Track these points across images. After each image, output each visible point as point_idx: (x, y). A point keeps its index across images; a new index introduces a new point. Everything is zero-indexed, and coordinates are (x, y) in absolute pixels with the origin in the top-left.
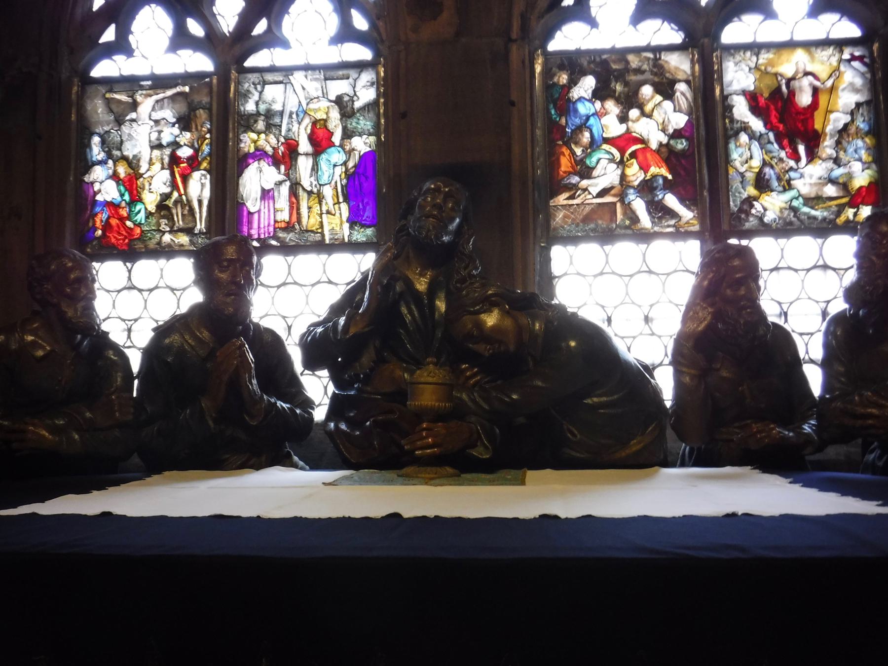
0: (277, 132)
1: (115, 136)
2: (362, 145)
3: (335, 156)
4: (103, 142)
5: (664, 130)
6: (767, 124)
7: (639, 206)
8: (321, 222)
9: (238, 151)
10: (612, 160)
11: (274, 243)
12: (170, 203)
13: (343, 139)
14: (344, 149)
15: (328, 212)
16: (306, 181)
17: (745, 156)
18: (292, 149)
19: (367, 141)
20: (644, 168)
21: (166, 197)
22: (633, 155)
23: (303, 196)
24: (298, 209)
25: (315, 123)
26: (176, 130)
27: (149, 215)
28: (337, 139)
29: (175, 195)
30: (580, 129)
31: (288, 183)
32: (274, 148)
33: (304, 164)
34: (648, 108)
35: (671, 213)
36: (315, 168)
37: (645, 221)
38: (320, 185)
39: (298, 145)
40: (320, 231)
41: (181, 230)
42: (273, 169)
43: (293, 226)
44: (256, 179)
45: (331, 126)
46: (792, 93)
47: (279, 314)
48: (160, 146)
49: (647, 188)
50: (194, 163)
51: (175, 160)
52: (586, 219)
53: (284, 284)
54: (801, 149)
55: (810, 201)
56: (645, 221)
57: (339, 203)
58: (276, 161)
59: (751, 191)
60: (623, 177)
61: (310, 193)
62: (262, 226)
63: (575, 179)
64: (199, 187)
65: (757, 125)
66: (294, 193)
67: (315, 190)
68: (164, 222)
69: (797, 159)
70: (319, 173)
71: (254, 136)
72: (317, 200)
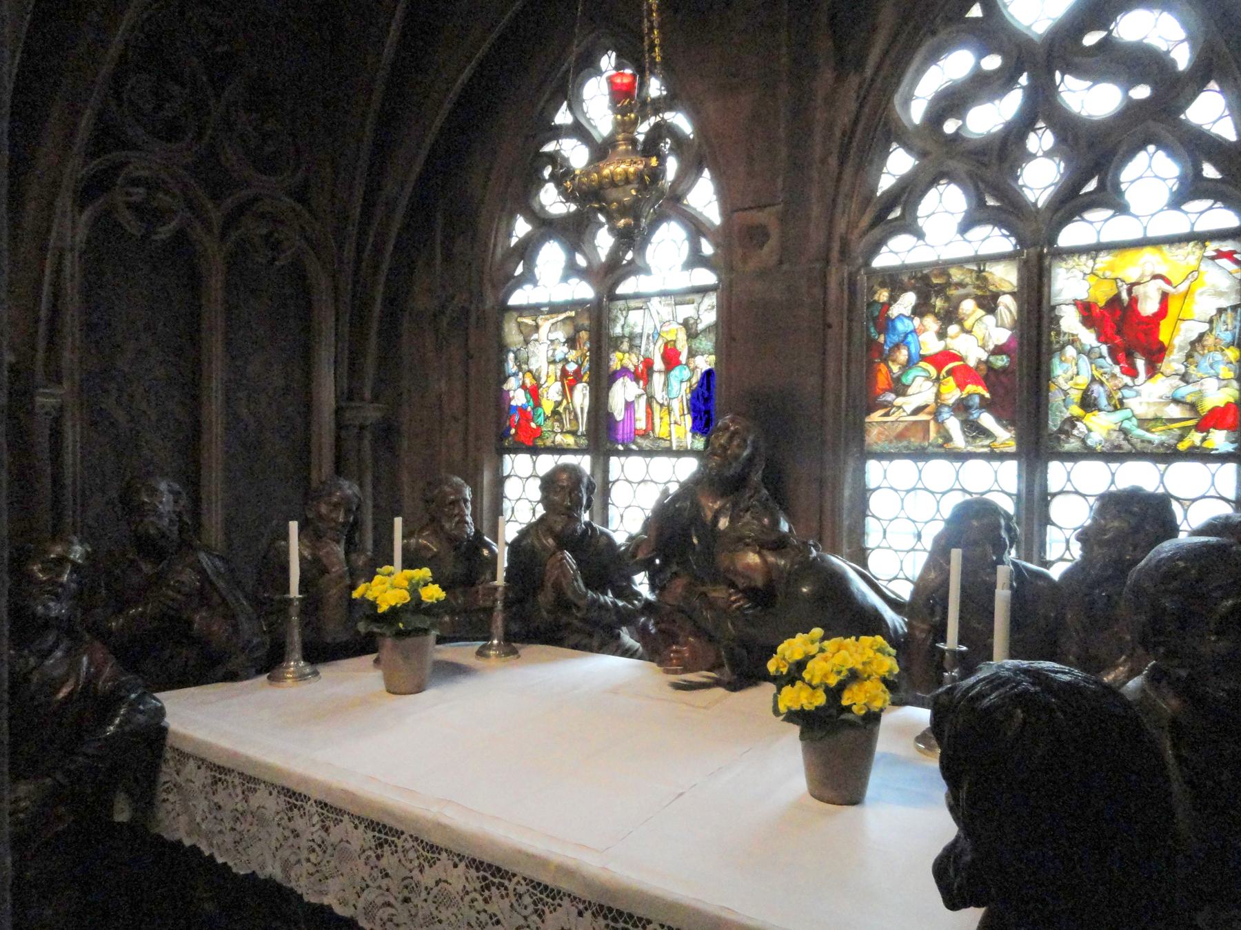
1: (523, 354)
2: (705, 363)
3: (678, 373)
4: (516, 358)
5: (983, 347)
6: (1101, 338)
7: (953, 425)
10: (928, 378)
11: (634, 447)
12: (561, 409)
16: (659, 394)
17: (1070, 373)
18: (648, 363)
20: (961, 386)
21: (558, 404)
22: (949, 373)
23: (656, 407)
25: (666, 345)
26: (565, 349)
27: (547, 418)
28: (683, 358)
29: (565, 402)
30: (897, 346)
33: (658, 379)
34: (967, 324)
35: (986, 433)
36: (666, 384)
37: (959, 441)
41: (568, 432)
44: (622, 393)
45: (679, 347)
46: (1134, 301)
48: (554, 362)
49: (962, 407)
50: (577, 377)
51: (564, 373)
52: (901, 436)
54: (1140, 363)
55: (1143, 422)
56: (959, 441)
58: (636, 377)
59: (1076, 410)
60: (938, 395)
61: (662, 405)
63: (890, 397)
64: (581, 397)
65: (1088, 337)
68: (557, 424)
69: (1133, 373)
71: (619, 355)
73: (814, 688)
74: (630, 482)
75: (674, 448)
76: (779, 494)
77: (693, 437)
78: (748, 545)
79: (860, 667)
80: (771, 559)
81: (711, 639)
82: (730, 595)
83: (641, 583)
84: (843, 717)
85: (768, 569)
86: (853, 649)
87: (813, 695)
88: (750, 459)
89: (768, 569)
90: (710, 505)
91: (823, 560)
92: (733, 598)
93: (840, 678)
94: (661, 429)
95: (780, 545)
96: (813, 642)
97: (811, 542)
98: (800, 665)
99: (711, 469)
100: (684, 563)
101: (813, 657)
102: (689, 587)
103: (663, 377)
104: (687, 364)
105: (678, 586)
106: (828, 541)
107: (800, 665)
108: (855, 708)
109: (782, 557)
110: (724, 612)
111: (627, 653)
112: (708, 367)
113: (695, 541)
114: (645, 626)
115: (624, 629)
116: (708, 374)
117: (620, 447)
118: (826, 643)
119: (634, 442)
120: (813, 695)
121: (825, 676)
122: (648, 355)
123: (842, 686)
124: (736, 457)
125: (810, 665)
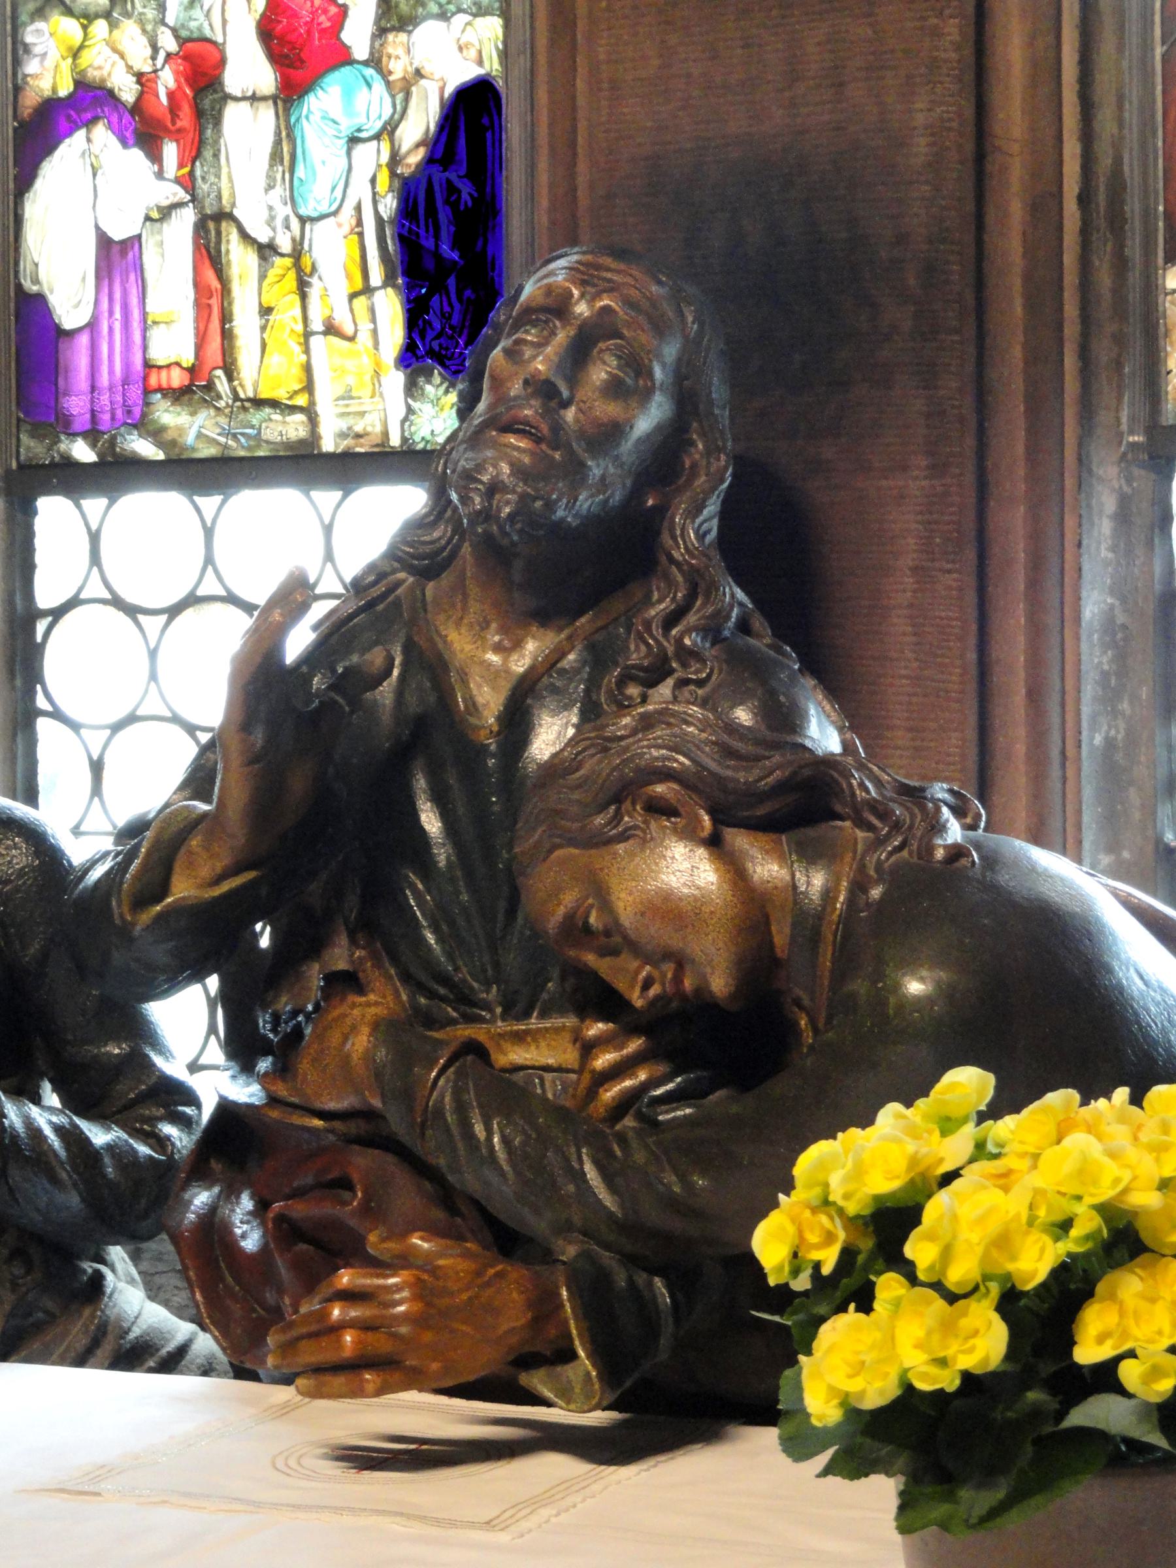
0: (151, 13)
3: (339, 103)
8: (308, 369)
9: (17, 90)
11: (145, 448)
13: (381, 32)
14: (384, 74)
15: (331, 329)
18: (202, 70)
19: (469, 36)
23: (241, 260)
24: (226, 317)
28: (357, 34)
31: (187, 218)
32: (140, 77)
33: (245, 131)
36: (285, 153)
38: (303, 220)
39: (222, 62)
40: (302, 400)
42: (136, 155)
43: (210, 387)
47: (176, 719)
53: (192, 600)
57: (367, 290)
58: (144, 130)
61: (266, 251)
62: (104, 379)
66: (209, 253)
67: (285, 245)
70: (300, 172)
71: (66, 27)
72: (291, 281)
73: (952, 1298)
74: (132, 611)
75: (328, 445)
76: (793, 587)
77: (411, 388)
78: (659, 809)
79: (1146, 1199)
80: (767, 869)
81: (506, 1240)
82: (588, 1049)
83: (185, 1027)
84: (1078, 1417)
85: (754, 909)
86: (1120, 1134)
87: (948, 1328)
88: (664, 463)
89: (754, 909)
90: (490, 661)
91: (991, 861)
92: (604, 1060)
93: (1071, 1245)
94: (265, 367)
95: (803, 805)
96: (947, 1125)
97: (939, 791)
98: (889, 1226)
99: (494, 489)
100: (381, 926)
101: (948, 1178)
102: (406, 1035)
103: (267, 114)
104: (376, 61)
105: (357, 1032)
106: (1014, 779)
107: (889, 1226)
108: (1129, 1373)
109: (810, 854)
110: (575, 1121)
111: (135, 1354)
112: (468, 73)
113: (431, 822)
114: (213, 1229)
115: (117, 1253)
116: (473, 107)
117: (82, 452)
118: (1006, 1127)
119: (144, 425)
120: (948, 1328)
121: (1003, 1242)
122: (197, 22)
123: (1071, 1288)
124: (608, 435)
125: (935, 1209)
